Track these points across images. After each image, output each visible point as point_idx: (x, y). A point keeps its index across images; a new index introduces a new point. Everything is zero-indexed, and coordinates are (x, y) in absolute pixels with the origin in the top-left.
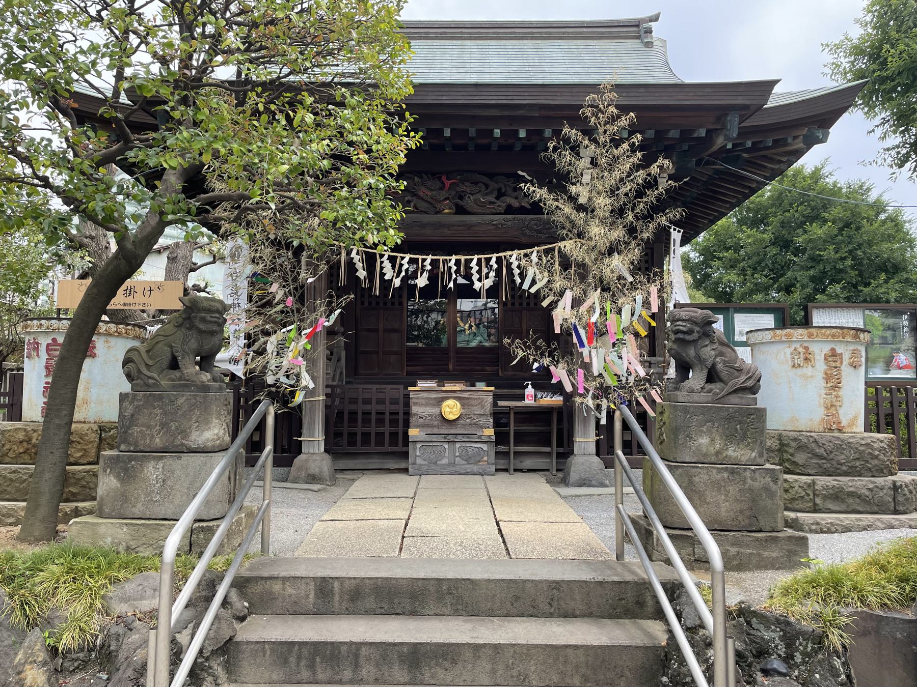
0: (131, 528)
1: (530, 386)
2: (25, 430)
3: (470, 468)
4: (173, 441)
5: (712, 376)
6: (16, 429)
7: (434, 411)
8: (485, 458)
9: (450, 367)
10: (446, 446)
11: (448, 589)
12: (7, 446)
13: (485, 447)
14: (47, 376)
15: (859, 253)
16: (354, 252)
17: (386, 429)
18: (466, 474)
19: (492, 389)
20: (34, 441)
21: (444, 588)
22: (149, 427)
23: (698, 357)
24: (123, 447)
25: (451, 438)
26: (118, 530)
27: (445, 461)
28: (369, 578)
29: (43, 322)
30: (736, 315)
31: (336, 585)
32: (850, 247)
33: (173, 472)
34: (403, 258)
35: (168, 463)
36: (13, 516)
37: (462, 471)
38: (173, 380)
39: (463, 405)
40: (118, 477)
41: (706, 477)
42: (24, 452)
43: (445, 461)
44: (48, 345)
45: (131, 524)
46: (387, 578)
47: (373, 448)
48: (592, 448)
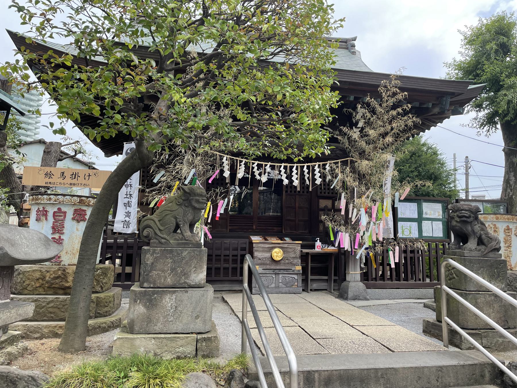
0: (158, 340)
1: (318, 241)
2: (41, 271)
3: (288, 290)
4: (180, 280)
5: (480, 242)
6: (34, 271)
7: (268, 255)
8: (296, 284)
9: (254, 227)
10: (274, 276)
11: (382, 375)
12: (27, 282)
13: (296, 277)
14: (53, 233)
15: (420, 169)
16: (225, 158)
17: (230, 265)
18: (286, 293)
19: (301, 242)
20: (47, 278)
21: (379, 374)
22: (163, 271)
23: (473, 231)
24: (146, 285)
25: (277, 271)
26: (149, 342)
27: (273, 285)
28: (336, 370)
29: (52, 197)
30: (424, 203)
31: (316, 375)
32: (416, 166)
33: (182, 301)
34: (266, 165)
35: (179, 295)
36: (38, 333)
37: (283, 291)
38: (178, 240)
39: (284, 252)
40: (145, 306)
41: (484, 299)
42: (40, 287)
43: (273, 285)
44: (54, 212)
45: (158, 338)
46: (346, 370)
47: (222, 278)
48: (358, 277)
